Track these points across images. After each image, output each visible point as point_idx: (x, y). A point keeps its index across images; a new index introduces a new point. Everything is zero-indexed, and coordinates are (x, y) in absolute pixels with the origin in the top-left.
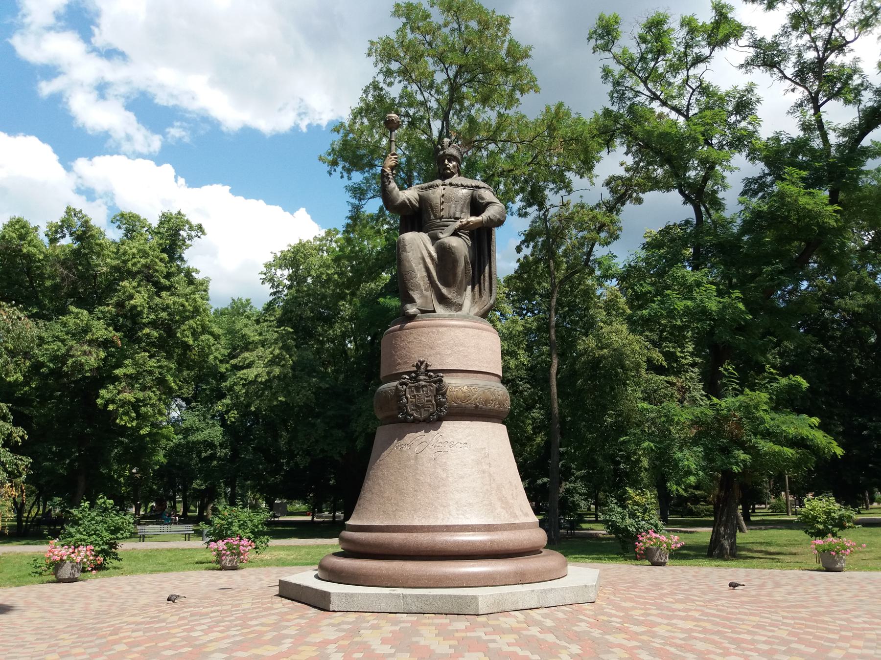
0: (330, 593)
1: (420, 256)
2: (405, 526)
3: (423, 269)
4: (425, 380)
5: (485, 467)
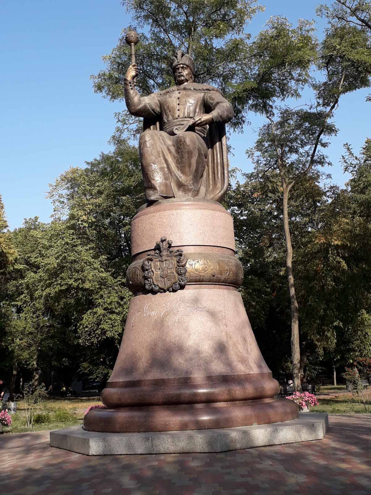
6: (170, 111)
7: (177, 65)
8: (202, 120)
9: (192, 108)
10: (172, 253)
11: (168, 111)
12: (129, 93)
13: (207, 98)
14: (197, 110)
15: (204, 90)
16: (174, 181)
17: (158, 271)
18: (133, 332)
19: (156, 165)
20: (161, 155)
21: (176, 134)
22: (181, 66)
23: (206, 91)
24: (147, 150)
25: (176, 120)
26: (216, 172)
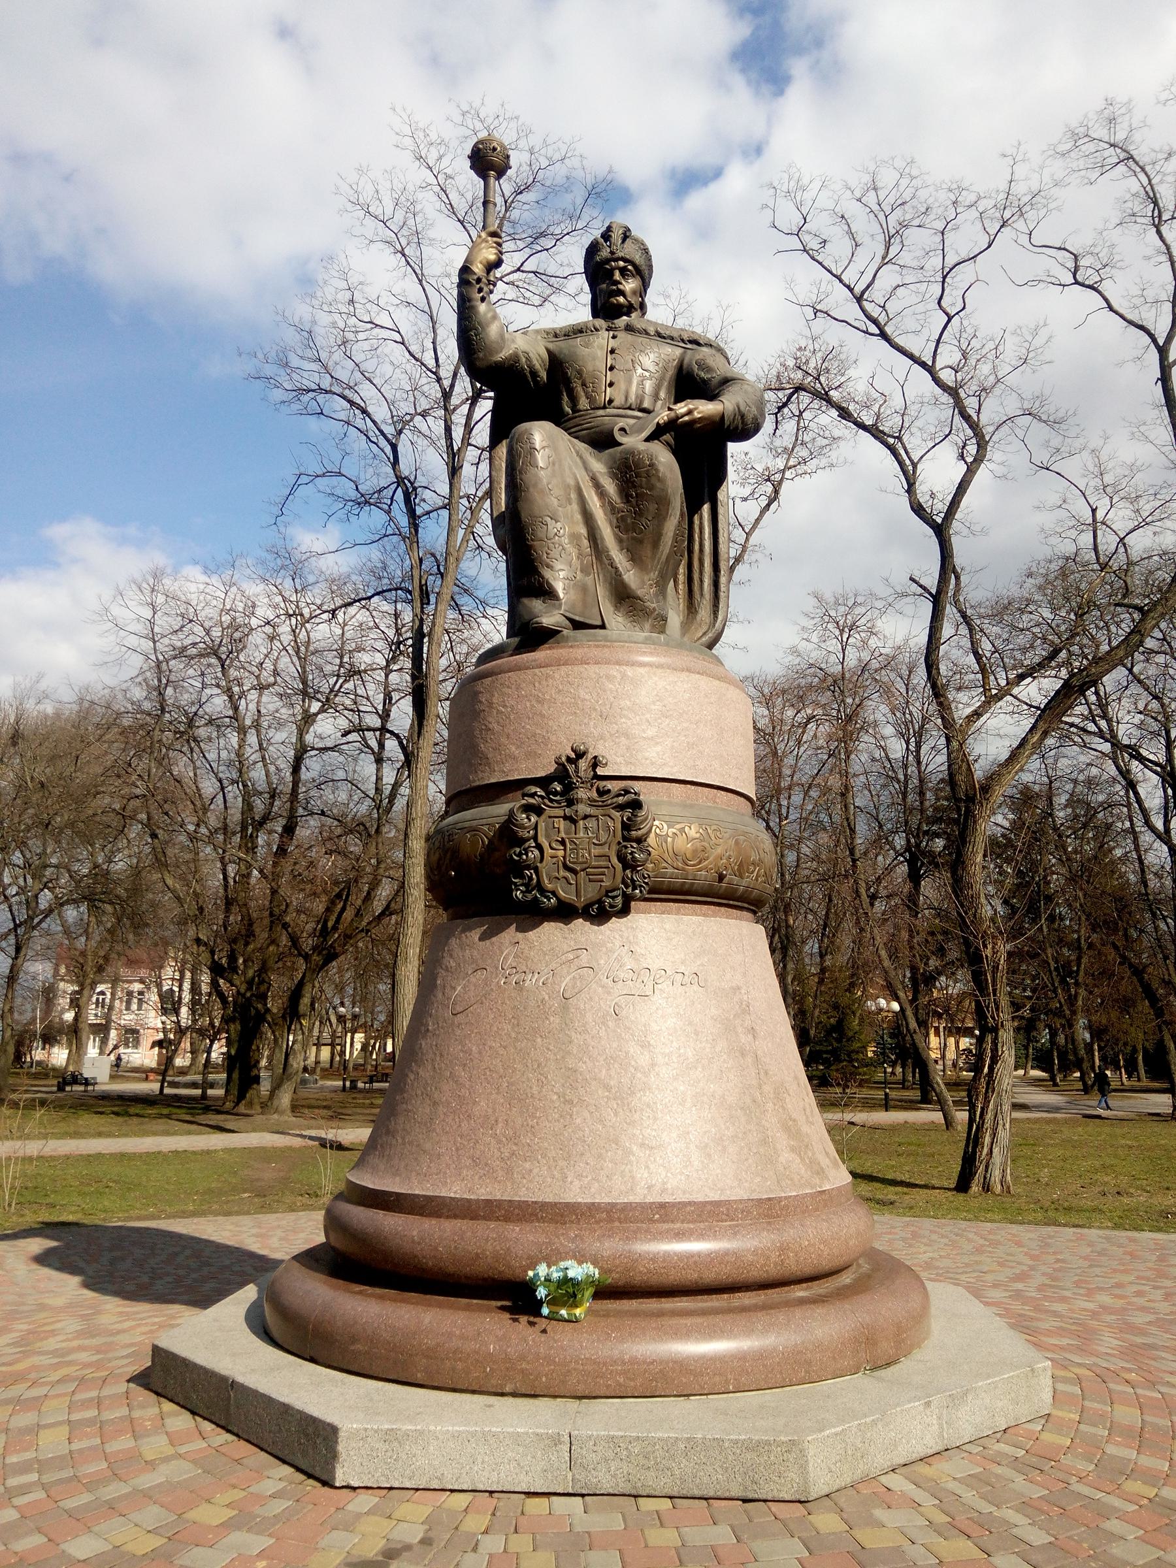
0: (334, 1430)
1: (572, 482)
2: (544, 1205)
3: (578, 517)
4: (592, 803)
5: (745, 1039)
6: (584, 385)
7: (608, 261)
8: (697, 415)
9: (649, 386)
10: (605, 798)
11: (577, 385)
12: (473, 308)
13: (690, 365)
14: (662, 395)
15: (683, 341)
16: (605, 581)
17: (557, 847)
18: (458, 1032)
19: (559, 525)
20: (573, 496)
21: (621, 444)
22: (621, 264)
23: (689, 346)
24: (536, 475)
25: (601, 412)
26: (696, 576)
